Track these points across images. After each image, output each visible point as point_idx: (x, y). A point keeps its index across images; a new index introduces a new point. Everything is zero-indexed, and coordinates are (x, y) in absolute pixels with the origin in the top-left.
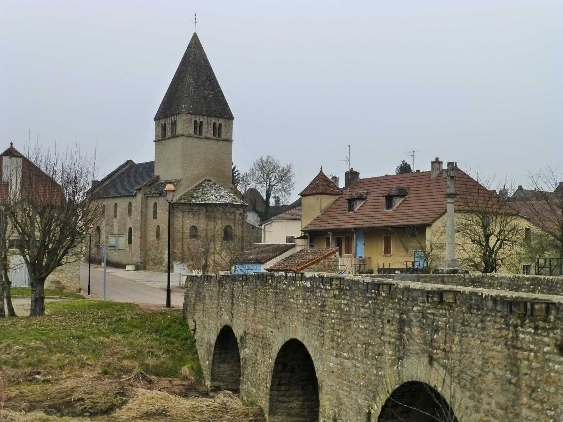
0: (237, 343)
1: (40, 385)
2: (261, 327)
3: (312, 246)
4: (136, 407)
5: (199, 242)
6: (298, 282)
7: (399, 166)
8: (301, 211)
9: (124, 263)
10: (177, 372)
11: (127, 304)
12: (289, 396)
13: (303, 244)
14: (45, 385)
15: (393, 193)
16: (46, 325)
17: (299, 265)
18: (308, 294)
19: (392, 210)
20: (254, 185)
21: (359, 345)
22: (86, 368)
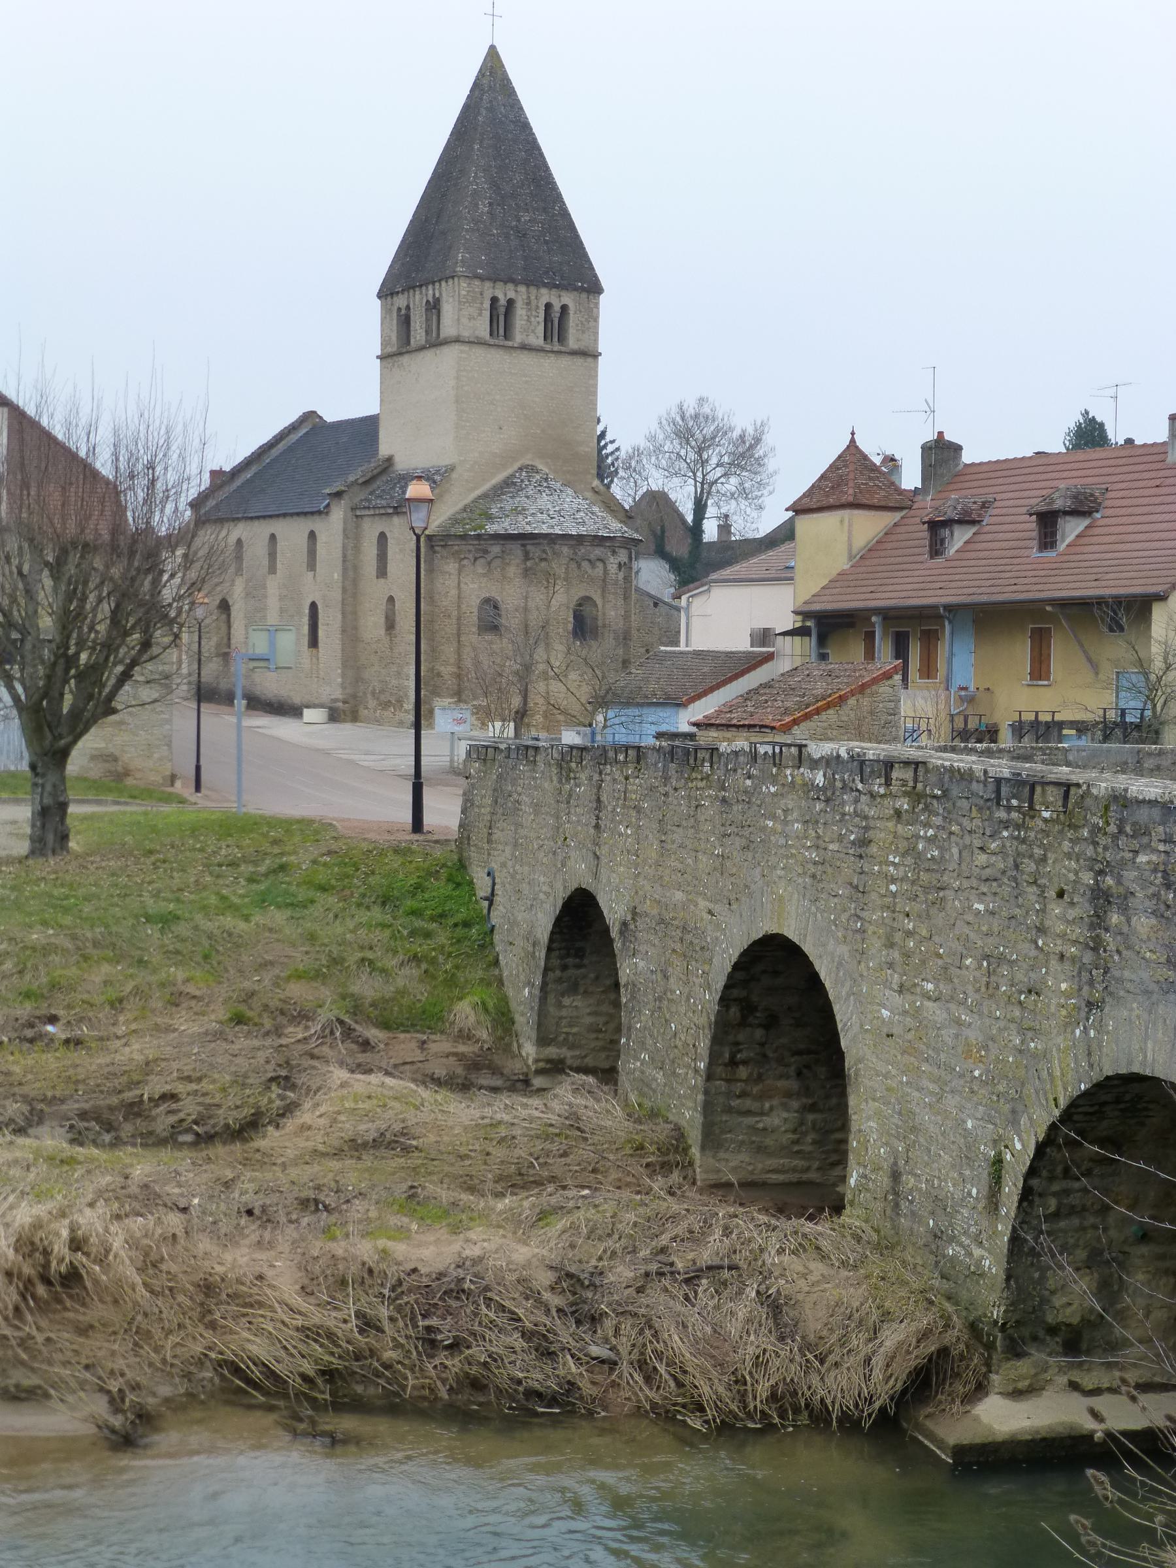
0: (611, 941)
1: (57, 1054)
2: (679, 896)
3: (823, 657)
4: (322, 1121)
5: (501, 644)
6: (788, 772)
7: (1072, 426)
8: (793, 554)
9: (297, 700)
10: (441, 1019)
11: (300, 821)
12: (761, 1097)
13: (798, 651)
14: (69, 1055)
15: (1058, 504)
16: (71, 885)
17: (787, 712)
18: (818, 806)
19: (1054, 554)
20: (660, 482)
21: (968, 962)
22: (184, 1005)
